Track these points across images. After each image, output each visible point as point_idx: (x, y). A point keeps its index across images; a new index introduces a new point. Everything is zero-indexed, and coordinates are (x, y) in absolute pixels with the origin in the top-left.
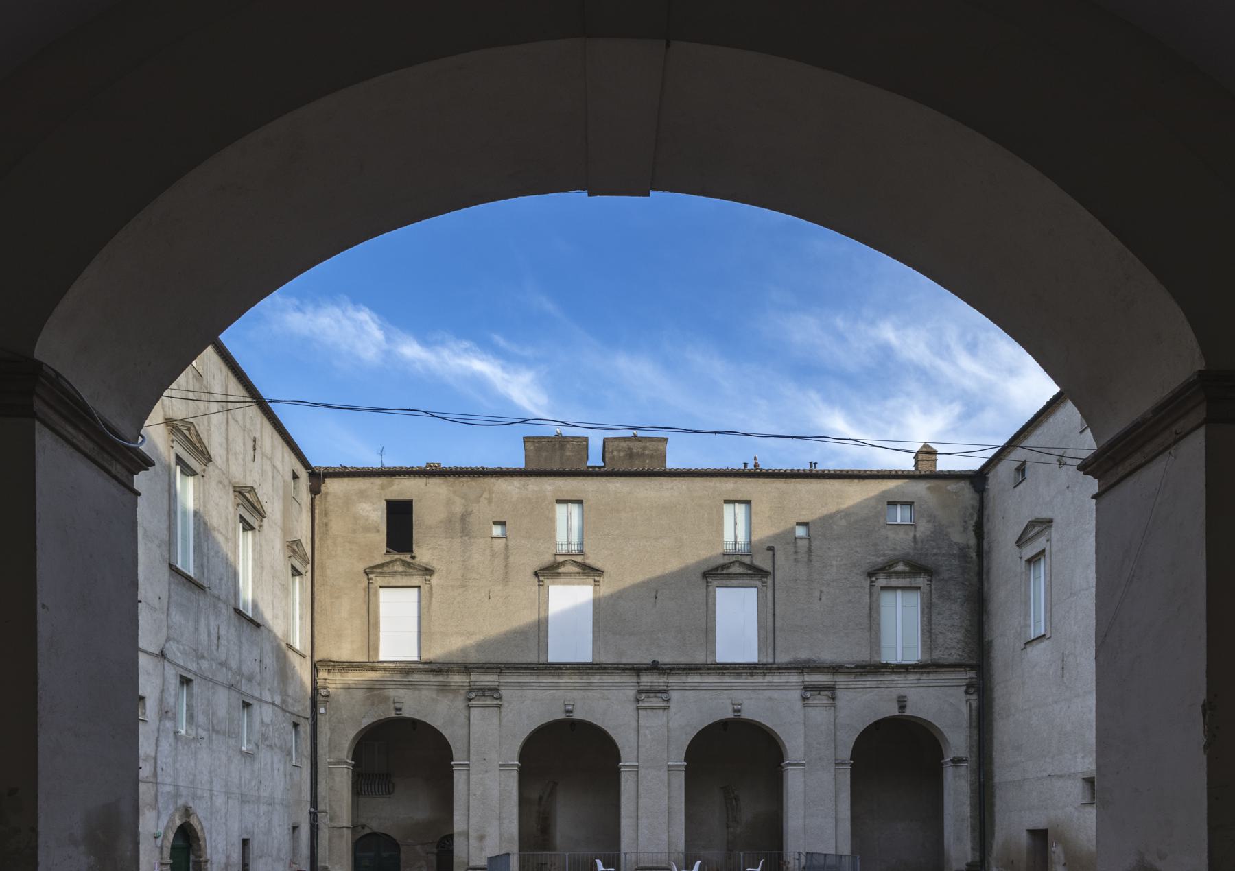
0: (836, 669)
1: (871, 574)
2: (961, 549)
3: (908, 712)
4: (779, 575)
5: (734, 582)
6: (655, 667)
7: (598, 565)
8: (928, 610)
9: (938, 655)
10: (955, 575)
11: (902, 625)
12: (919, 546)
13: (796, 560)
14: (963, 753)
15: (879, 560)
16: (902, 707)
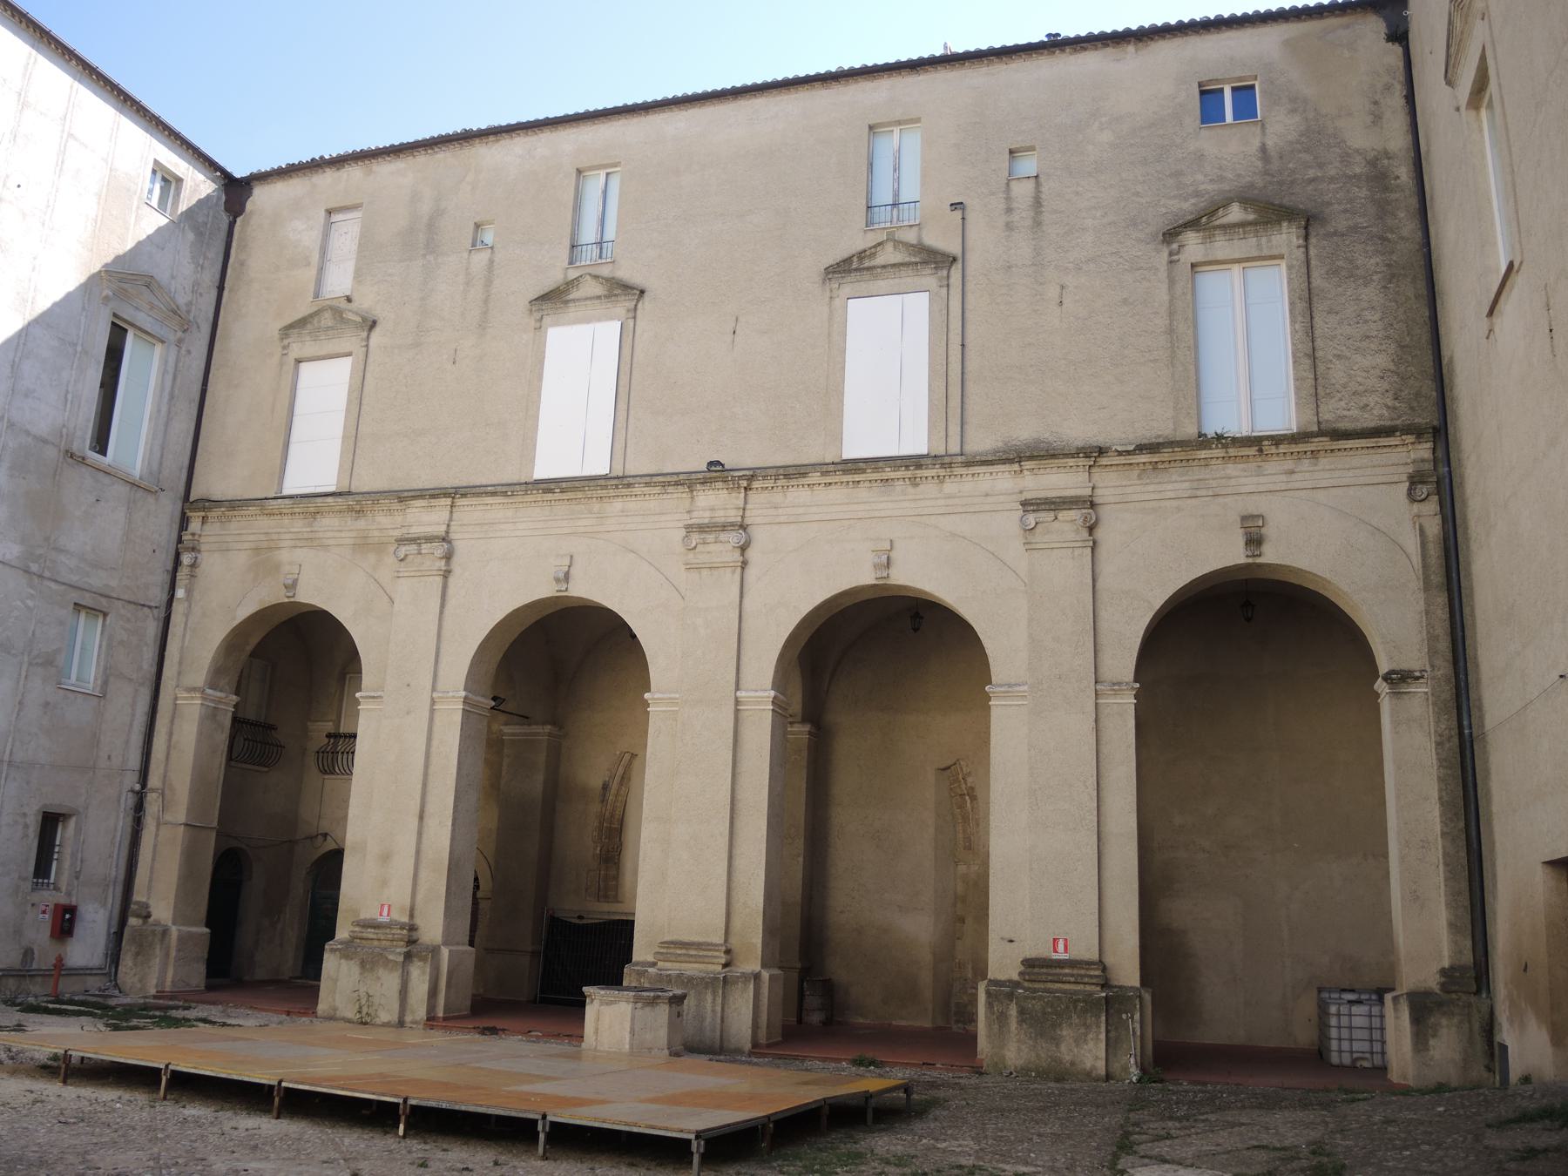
0: (1095, 454)
1: (1171, 235)
2: (1373, 163)
3: (1271, 555)
4: (974, 261)
5: (882, 284)
6: (716, 472)
7: (636, 279)
8: (1306, 303)
9: (1336, 411)
10: (1362, 221)
11: (1250, 341)
12: (1275, 165)
13: (1009, 227)
14: (1414, 659)
15: (1186, 206)
16: (1254, 541)
